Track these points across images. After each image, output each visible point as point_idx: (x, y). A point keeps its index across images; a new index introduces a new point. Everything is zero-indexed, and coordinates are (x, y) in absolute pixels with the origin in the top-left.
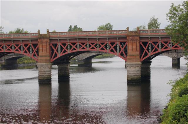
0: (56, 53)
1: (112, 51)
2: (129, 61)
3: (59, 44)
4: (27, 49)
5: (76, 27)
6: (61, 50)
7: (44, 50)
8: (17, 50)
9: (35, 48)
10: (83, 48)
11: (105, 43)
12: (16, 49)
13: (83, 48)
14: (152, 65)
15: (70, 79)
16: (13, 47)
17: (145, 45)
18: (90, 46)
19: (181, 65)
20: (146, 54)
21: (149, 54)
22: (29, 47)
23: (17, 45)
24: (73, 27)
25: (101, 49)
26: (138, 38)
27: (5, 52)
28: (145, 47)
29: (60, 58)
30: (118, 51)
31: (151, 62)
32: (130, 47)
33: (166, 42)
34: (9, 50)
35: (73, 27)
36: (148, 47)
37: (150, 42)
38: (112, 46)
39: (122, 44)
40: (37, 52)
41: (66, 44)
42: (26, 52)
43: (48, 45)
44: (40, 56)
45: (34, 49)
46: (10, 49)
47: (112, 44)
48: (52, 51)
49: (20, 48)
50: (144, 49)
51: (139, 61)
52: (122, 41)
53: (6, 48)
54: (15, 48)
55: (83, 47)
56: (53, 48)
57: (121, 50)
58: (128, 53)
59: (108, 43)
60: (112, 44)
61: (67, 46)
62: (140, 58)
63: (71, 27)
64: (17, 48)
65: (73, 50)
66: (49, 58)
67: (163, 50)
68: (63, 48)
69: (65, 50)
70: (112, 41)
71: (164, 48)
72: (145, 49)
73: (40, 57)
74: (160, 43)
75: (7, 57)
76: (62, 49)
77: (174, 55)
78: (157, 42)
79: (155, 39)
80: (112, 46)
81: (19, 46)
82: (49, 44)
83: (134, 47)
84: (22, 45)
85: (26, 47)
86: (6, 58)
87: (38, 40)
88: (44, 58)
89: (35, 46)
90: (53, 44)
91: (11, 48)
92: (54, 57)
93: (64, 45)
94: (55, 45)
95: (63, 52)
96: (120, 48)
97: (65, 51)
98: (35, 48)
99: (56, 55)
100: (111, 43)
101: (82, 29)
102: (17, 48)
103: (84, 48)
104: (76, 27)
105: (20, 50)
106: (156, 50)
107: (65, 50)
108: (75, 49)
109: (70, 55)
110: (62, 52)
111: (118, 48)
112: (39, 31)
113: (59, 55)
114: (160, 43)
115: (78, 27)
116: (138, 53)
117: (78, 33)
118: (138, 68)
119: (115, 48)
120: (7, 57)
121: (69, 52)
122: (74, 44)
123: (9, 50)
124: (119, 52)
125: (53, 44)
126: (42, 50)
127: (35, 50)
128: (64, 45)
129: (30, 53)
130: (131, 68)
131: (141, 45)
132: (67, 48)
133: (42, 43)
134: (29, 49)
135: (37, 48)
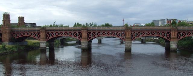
3: (16, 33)
4: (164, 34)
5: (78, 24)
7: (43, 35)
10: (61, 35)
14: (92, 42)
18: (65, 34)
19: (102, 43)
20: (90, 38)
21: (92, 38)
23: (70, 33)
24: (77, 24)
26: (177, 30)
27: (32, 37)
29: (50, 39)
32: (83, 35)
33: (99, 33)
35: (77, 24)
40: (40, 36)
43: (45, 33)
47: (75, 33)
48: (47, 36)
56: (13, 34)
59: (32, 33)
60: (75, 33)
63: (76, 23)
64: (70, 34)
65: (184, 36)
66: (45, 39)
70: (74, 31)
72: (48, 35)
74: (186, 32)
75: (61, 38)
76: (51, 35)
78: (185, 32)
79: (139, 31)
82: (46, 33)
83: (175, 34)
84: (73, 33)
85: (163, 33)
86: (61, 39)
88: (43, 39)
89: (39, 33)
90: (47, 33)
92: (89, 39)
93: (53, 33)
95: (184, 36)
96: (167, 35)
97: (18, 36)
99: (49, 38)
102: (70, 34)
104: (78, 24)
106: (95, 36)
111: (166, 35)
113: (50, 38)
115: (79, 23)
116: (176, 37)
118: (86, 44)
119: (76, 35)
120: (61, 38)
121: (55, 36)
122: (18, 33)
125: (47, 33)
127: (39, 36)
128: (53, 33)
131: (88, 34)
132: (54, 35)
133: (128, 31)
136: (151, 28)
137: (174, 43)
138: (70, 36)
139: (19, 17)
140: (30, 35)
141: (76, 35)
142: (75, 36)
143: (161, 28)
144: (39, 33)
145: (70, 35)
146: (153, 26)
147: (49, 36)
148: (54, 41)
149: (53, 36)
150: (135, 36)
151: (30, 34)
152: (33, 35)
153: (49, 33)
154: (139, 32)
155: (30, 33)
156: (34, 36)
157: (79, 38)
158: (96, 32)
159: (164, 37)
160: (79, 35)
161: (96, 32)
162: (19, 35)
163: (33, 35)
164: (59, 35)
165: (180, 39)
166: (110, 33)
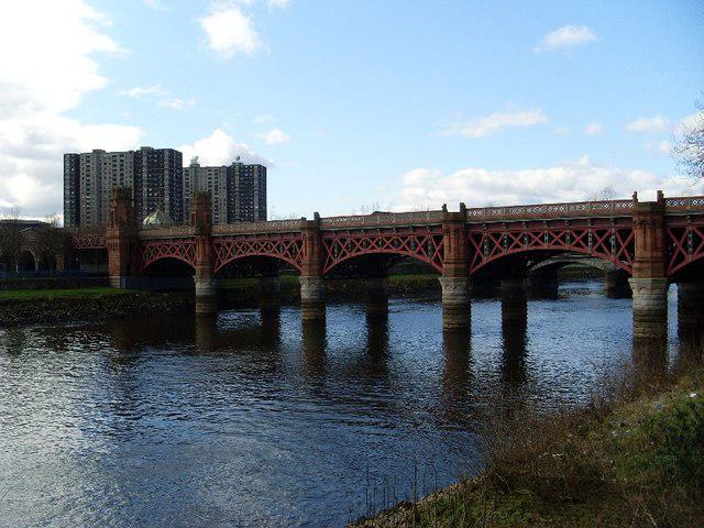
1: (600, 249)
6: (491, 248)
9: (437, 245)
15: (530, 330)
17: (497, 239)
22: (427, 242)
32: (639, 242)
36: (686, 242)
46: (560, 241)
47: (601, 233)
49: (585, 239)
52: (622, 225)
53: (384, 243)
62: (666, 266)
70: (599, 226)
78: (605, 231)
91: (563, 238)
98: (437, 245)
99: (681, 258)
110: (698, 250)
111: (590, 239)
112: (445, 206)
125: (672, 230)
127: (623, 246)
128: (497, 236)
138: (578, 249)
139: (74, 163)
141: (426, 249)
144: (631, 231)
145: (578, 245)
147: (685, 246)
148: (306, 324)
150: (686, 250)
152: (416, 246)
155: (388, 239)
156: (420, 253)
159: (582, 247)
163: (416, 246)
165: (684, 264)
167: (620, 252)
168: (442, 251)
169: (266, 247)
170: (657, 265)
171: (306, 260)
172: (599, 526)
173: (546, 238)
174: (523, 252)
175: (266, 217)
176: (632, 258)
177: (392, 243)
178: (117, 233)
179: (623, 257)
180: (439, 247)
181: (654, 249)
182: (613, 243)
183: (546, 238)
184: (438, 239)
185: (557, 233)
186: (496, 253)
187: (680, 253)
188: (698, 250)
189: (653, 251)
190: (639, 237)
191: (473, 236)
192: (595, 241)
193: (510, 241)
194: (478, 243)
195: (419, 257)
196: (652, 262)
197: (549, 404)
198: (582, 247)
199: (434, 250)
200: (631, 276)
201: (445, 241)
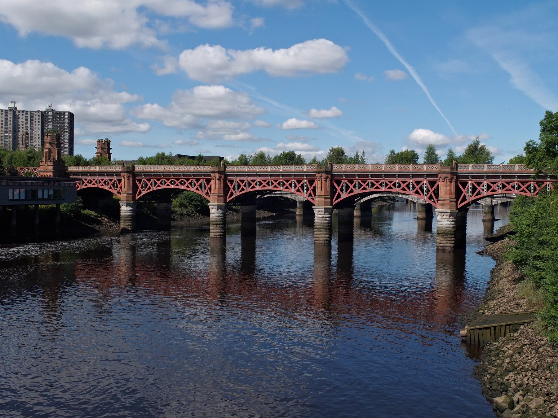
0: (339, 193)
2: (441, 207)
8: (287, 188)
9: (208, 185)
10: (377, 188)
11: (290, 181)
12: (285, 186)
13: (377, 188)
16: (281, 184)
18: (386, 185)
20: (464, 199)
25: (402, 190)
28: (339, 186)
30: (425, 193)
31: (468, 209)
33: (479, 183)
34: (276, 187)
36: (234, 187)
37: (344, 181)
38: (352, 184)
39: (432, 184)
40: (314, 190)
41: (354, 181)
42: (298, 190)
44: (442, 199)
45: (309, 187)
46: (277, 185)
47: (418, 183)
50: (462, 192)
51: (455, 208)
53: (175, 183)
54: (175, 183)
55: (377, 186)
57: (430, 191)
58: (439, 196)
59: (411, 181)
61: (246, 183)
62: (332, 199)
67: (489, 193)
68: (349, 187)
69: (352, 189)
71: (252, 188)
72: (338, 189)
73: (318, 197)
77: (487, 201)
80: (352, 184)
81: (407, 183)
85: (299, 184)
87: (316, 175)
91: (279, 184)
94: (339, 183)
96: (428, 189)
97: (352, 191)
98: (208, 185)
100: (415, 182)
101: (418, 156)
103: (266, 187)
105: (292, 187)
107: (352, 189)
108: (366, 189)
109: (356, 196)
110: (239, 190)
114: (357, 181)
117: (384, 167)
121: (357, 191)
123: (276, 186)
124: (427, 195)
125: (336, 182)
126: (320, 188)
127: (431, 190)
129: (304, 191)
130: (444, 217)
132: (354, 187)
134: (302, 187)
135: (314, 185)
136: (383, 171)
137: (444, 213)
138: (287, 190)
140: (187, 187)
142: (417, 192)
143: (501, 169)
145: (403, 189)
146: (363, 163)
149: (243, 190)
151: (287, 184)
153: (233, 181)
154: (351, 182)
157: (430, 198)
158: (485, 183)
159: (406, 190)
160: (431, 191)
161: (485, 183)
162: (245, 186)
163: (195, 185)
164: (370, 189)
166: (513, 187)
167: (429, 194)
168: (210, 189)
169: (180, 183)
170: (220, 198)
171: (125, 190)
172: (557, 278)
173: (384, 185)
174: (153, 191)
175: (73, 154)
176: (315, 195)
177: (96, 182)
178: (51, 168)
179: (310, 195)
180: (209, 186)
181: (451, 193)
182: (425, 189)
183: (384, 185)
184: (208, 181)
185: (188, 180)
186: (478, 194)
187: (232, 192)
188: (239, 190)
189: (450, 194)
190: (318, 183)
191: (461, 183)
192: (414, 187)
193: (347, 187)
194: (232, 184)
195: (197, 192)
196: (218, 196)
197: (178, 233)
198: (406, 190)
199: (205, 188)
200: (314, 205)
201: (212, 183)
